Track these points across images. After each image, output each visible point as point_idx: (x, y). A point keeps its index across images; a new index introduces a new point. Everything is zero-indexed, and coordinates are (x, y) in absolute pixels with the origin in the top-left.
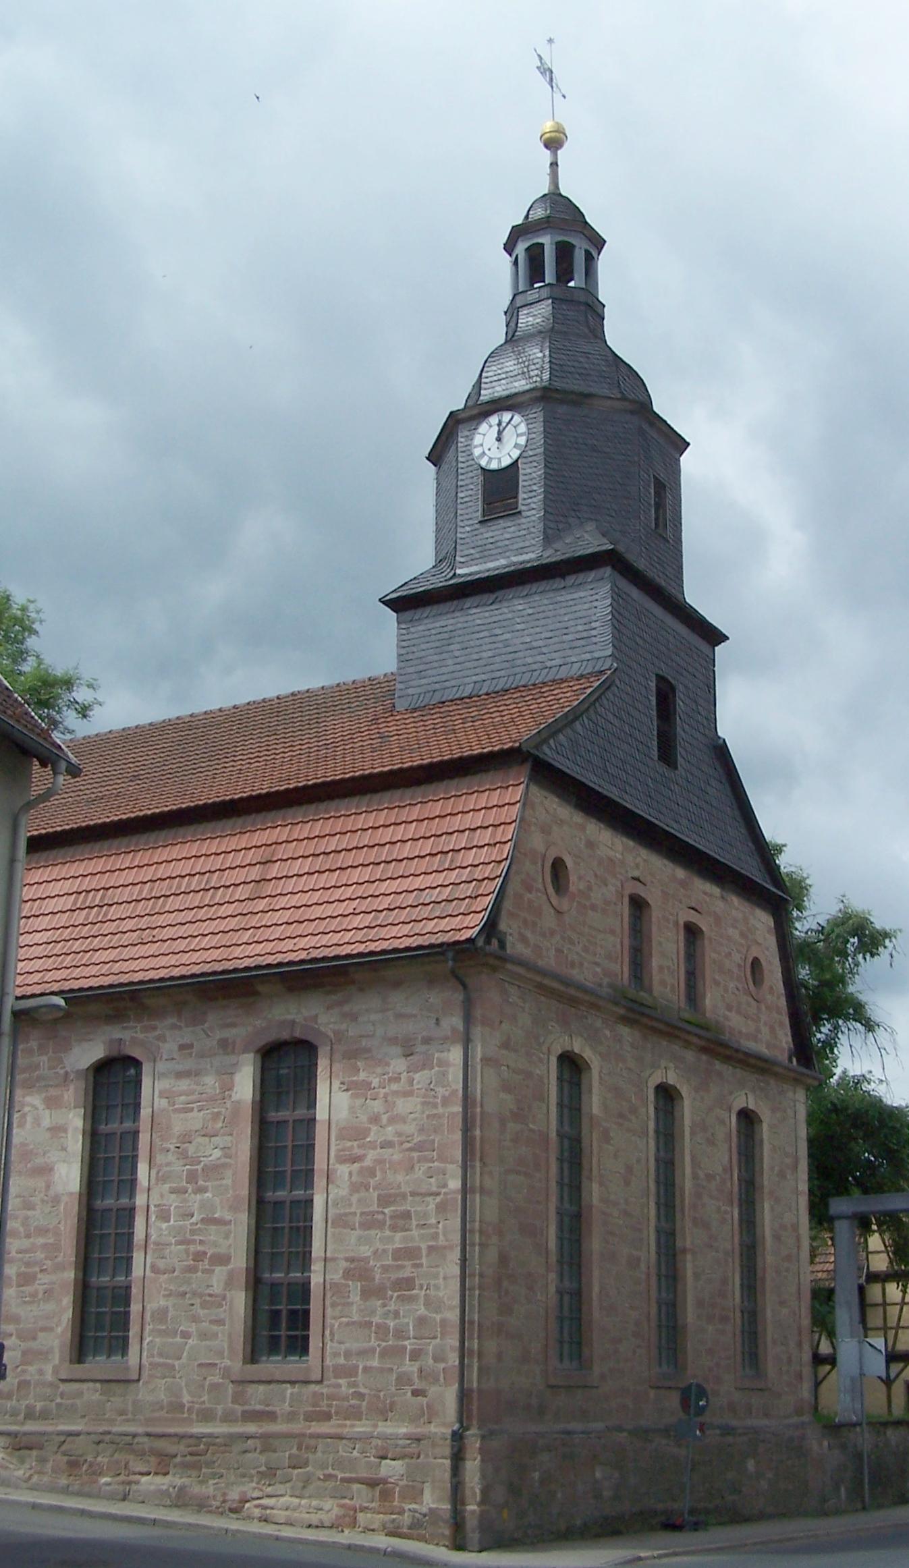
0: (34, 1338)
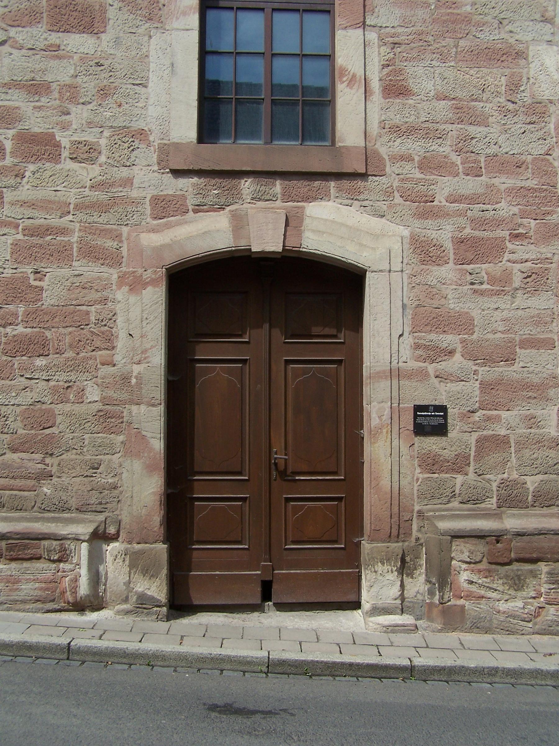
0: (510, 359)
